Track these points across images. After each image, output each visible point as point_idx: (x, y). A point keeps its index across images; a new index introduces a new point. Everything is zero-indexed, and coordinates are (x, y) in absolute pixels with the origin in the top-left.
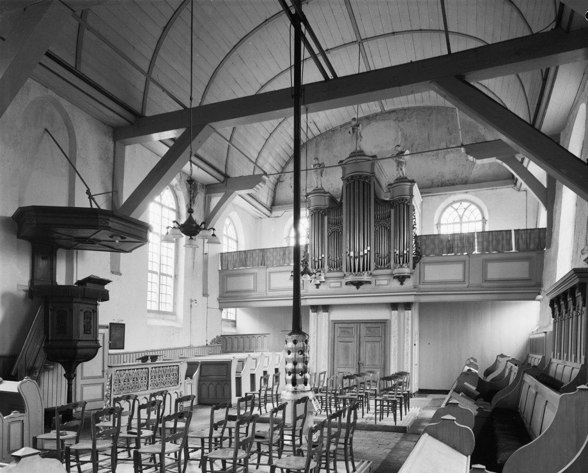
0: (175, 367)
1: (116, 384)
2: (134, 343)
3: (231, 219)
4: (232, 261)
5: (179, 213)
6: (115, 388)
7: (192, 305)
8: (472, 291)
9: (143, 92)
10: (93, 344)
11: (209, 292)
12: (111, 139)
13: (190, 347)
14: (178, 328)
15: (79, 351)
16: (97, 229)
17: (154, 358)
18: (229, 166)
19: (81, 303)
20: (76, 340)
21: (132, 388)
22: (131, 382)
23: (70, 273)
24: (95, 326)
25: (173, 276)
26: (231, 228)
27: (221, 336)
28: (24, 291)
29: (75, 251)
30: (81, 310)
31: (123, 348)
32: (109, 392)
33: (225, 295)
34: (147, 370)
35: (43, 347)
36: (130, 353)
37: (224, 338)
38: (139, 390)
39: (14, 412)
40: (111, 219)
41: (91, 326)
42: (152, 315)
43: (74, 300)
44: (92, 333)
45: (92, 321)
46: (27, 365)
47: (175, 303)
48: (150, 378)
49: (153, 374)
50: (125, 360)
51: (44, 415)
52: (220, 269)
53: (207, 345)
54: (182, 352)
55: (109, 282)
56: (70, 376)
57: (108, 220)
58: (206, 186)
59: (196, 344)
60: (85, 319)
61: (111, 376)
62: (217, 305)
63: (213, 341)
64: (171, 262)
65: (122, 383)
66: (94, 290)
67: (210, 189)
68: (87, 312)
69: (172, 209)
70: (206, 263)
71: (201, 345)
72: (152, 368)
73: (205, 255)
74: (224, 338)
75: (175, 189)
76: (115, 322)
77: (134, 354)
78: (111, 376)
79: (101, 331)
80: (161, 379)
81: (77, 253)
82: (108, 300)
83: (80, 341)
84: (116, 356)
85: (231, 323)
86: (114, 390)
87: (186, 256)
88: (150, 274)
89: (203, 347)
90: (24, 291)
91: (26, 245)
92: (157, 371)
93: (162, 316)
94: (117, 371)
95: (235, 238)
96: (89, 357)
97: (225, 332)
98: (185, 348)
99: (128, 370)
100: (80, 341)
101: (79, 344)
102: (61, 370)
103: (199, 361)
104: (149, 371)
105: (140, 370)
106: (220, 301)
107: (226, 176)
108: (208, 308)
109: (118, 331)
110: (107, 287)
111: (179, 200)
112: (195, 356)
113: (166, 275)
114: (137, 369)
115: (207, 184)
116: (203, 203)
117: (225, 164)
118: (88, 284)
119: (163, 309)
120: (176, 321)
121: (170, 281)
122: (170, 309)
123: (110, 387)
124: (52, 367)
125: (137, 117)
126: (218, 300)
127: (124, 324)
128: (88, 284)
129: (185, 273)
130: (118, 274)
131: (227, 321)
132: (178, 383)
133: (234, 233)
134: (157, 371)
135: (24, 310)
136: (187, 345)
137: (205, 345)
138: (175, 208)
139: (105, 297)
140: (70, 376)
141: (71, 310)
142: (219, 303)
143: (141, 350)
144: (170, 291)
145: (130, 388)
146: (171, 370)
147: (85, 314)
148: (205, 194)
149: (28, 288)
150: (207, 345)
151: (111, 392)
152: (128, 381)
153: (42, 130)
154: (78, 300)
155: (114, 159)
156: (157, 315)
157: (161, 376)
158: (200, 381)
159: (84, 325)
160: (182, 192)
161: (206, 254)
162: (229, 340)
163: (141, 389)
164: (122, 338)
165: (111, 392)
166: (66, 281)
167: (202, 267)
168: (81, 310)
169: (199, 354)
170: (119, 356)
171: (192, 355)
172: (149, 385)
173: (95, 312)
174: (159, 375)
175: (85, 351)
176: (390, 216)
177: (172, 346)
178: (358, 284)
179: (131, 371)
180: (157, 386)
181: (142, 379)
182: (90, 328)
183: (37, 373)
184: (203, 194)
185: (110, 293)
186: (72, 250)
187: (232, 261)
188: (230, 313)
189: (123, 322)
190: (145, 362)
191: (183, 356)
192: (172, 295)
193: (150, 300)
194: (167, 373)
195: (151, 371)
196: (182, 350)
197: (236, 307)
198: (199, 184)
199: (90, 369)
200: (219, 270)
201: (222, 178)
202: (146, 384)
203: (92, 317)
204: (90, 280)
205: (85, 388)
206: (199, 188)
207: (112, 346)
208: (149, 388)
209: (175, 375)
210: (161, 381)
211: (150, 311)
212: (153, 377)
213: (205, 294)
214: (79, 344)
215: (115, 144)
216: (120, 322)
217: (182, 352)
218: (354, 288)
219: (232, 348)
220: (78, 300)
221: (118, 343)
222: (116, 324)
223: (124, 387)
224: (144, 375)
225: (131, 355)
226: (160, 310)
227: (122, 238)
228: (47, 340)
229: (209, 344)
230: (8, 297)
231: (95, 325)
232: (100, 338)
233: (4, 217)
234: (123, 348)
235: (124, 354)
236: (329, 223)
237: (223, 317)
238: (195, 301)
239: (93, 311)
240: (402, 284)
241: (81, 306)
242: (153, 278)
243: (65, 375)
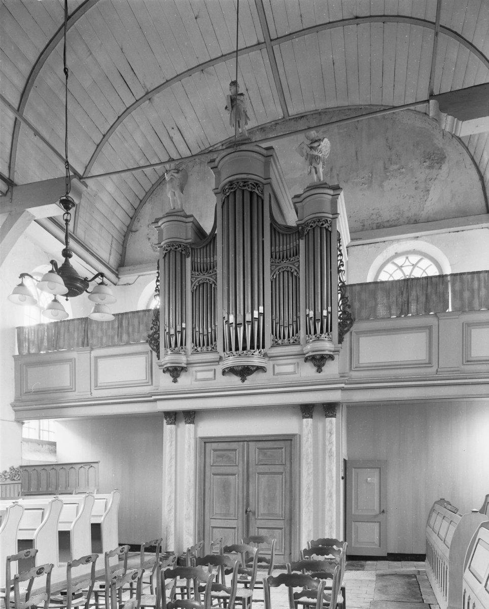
27: (21, 467)
52: (17, 353)
74: (72, 467)
142: (15, 411)
171: (307, 447)
176: (297, 253)
178: (244, 372)
200: (14, 356)
218: (235, 380)
236: (193, 269)
240: (175, 381)
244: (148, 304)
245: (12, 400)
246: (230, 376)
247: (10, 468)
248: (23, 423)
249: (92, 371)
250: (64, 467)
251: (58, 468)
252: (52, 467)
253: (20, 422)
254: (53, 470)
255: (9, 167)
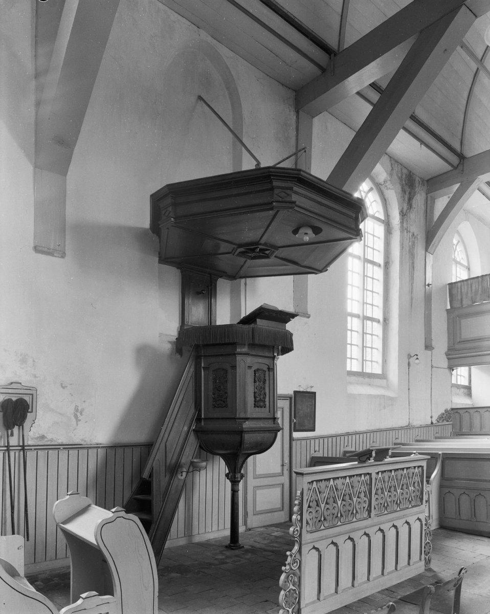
0: (416, 470)
1: (310, 510)
2: (329, 421)
3: (460, 236)
4: (469, 292)
5: (389, 225)
6: (308, 518)
7: (411, 363)
8: (40, 446)
9: (340, 13)
10: (269, 424)
11: (434, 344)
12: (292, 109)
13: (409, 427)
14: (391, 399)
15: (247, 437)
16: (272, 209)
17: (382, 454)
18: (465, 142)
19: (247, 354)
20: (242, 419)
21: (341, 515)
22: (339, 503)
23: (236, 306)
24: (272, 394)
25: (381, 320)
26: (460, 248)
27: (452, 409)
28: (170, 342)
29: (243, 281)
30: (250, 367)
31: (314, 430)
32: (298, 529)
33: (457, 346)
34: (368, 477)
35: (194, 430)
36: (323, 437)
37: (457, 412)
38: (355, 520)
39: (84, 595)
40: (295, 188)
41: (265, 394)
42: (353, 379)
43: (238, 350)
44: (267, 403)
45: (267, 385)
46: (168, 461)
47: (385, 361)
48: (374, 492)
49: (380, 484)
50: (317, 449)
51: (157, 594)
52: (449, 307)
53: (432, 423)
54: (397, 434)
55: (293, 316)
56: (235, 475)
57: (291, 189)
58: (428, 181)
59: (417, 423)
60: (255, 382)
61: (302, 493)
62: (445, 363)
63: (441, 418)
64: (379, 300)
65: (323, 506)
66: (269, 333)
67: (434, 183)
68: (258, 370)
69: (378, 219)
70: (428, 298)
71: (423, 423)
72: (378, 473)
73: (427, 287)
74: (457, 412)
75: (383, 188)
76: (301, 390)
77: (330, 439)
78: (302, 493)
79: (281, 404)
80: (392, 496)
81: (245, 284)
82: (293, 350)
83: (247, 419)
84: (304, 442)
85: (462, 390)
86: (307, 523)
87: (401, 288)
88: (349, 318)
89: (427, 426)
90: (170, 342)
91: (173, 275)
92: (386, 479)
93: (367, 380)
94: (312, 482)
95: (466, 264)
96: (262, 448)
97: (457, 404)
98: (402, 428)
99: (334, 479)
100: (247, 419)
101: (247, 425)
102: (220, 467)
103: (440, 453)
104: (371, 479)
105: (355, 479)
106: (449, 357)
107: (461, 157)
108: (432, 367)
109: (304, 404)
110: (289, 326)
111: (388, 206)
112: (417, 441)
113: (372, 319)
114: (350, 477)
115: (430, 177)
116: (423, 207)
117: (460, 137)
118: (258, 320)
119: (368, 370)
120: (388, 387)
121: (378, 329)
122: (378, 370)
123: (299, 517)
124: (204, 464)
125: (332, 55)
126: (447, 354)
127: (315, 393)
128: (258, 320)
129: (400, 316)
130: (304, 317)
131: (458, 386)
132: (422, 499)
133: (465, 257)
134: (386, 479)
135: (168, 371)
136: (404, 423)
137: (429, 423)
138: (382, 217)
139: (287, 348)
140: (235, 475)
141: (234, 367)
142: (449, 359)
143: (340, 432)
144: (378, 343)
145: (337, 517)
146: (411, 475)
147: (255, 374)
148: (427, 194)
149: (174, 339)
150: (432, 423)
151: (301, 528)
152: (334, 502)
153: (193, 99)
154: (245, 350)
155: (297, 139)
156: (361, 379)
157: (393, 489)
158: (441, 487)
159: (255, 393)
160: (393, 191)
161: (428, 285)
162: (466, 417)
163: (358, 516)
164: (313, 416)
165: (301, 528)
166: (231, 321)
167: (423, 305)
168: (250, 367)
169: (422, 438)
170: (308, 441)
171: (411, 440)
172: (373, 508)
173: (271, 369)
174: (390, 487)
175: (258, 437)
177: (383, 426)
179: (339, 482)
180: (386, 508)
181: (358, 497)
182: (265, 398)
183: (184, 474)
184: (424, 195)
185: (294, 338)
186: (239, 280)
187: (469, 292)
188: (461, 375)
189: (313, 390)
190: (364, 462)
191: (398, 441)
192: (381, 349)
193: (350, 357)
194: (404, 481)
195: (376, 479)
196: (397, 431)
197: (469, 365)
198: (417, 179)
199: (264, 464)
200: (447, 310)
201: (455, 160)
202: (366, 506)
203: (267, 378)
204: (263, 313)
205: (259, 492)
206: (417, 185)
207: (297, 427)
208: (373, 513)
209: (416, 484)
210: (393, 498)
211: (351, 373)
212: (380, 491)
213: (429, 347)
214: (247, 425)
215: (298, 117)
216: (309, 390)
217: (397, 434)
219: (471, 426)
220: (245, 350)
221: (306, 421)
222: (303, 392)
223: (326, 514)
224: (363, 488)
225: (326, 440)
226: (364, 371)
227: (317, 230)
228: (199, 419)
229: (434, 422)
230: (143, 352)
231: (272, 391)
232: (279, 415)
233: (137, 228)
234: (314, 430)
235: (315, 438)
237: (453, 382)
238: (416, 357)
239: (269, 369)
241: (249, 360)
242: (354, 324)
243: (227, 475)
244: (368, 198)
245: (446, 349)
246: (178, 328)
247: (445, 411)
248: (453, 370)
249: (16, 476)
250: (478, 410)
251: (472, 411)
252: (476, 410)
253: (451, 368)
254: (467, 413)
255: (461, 143)
